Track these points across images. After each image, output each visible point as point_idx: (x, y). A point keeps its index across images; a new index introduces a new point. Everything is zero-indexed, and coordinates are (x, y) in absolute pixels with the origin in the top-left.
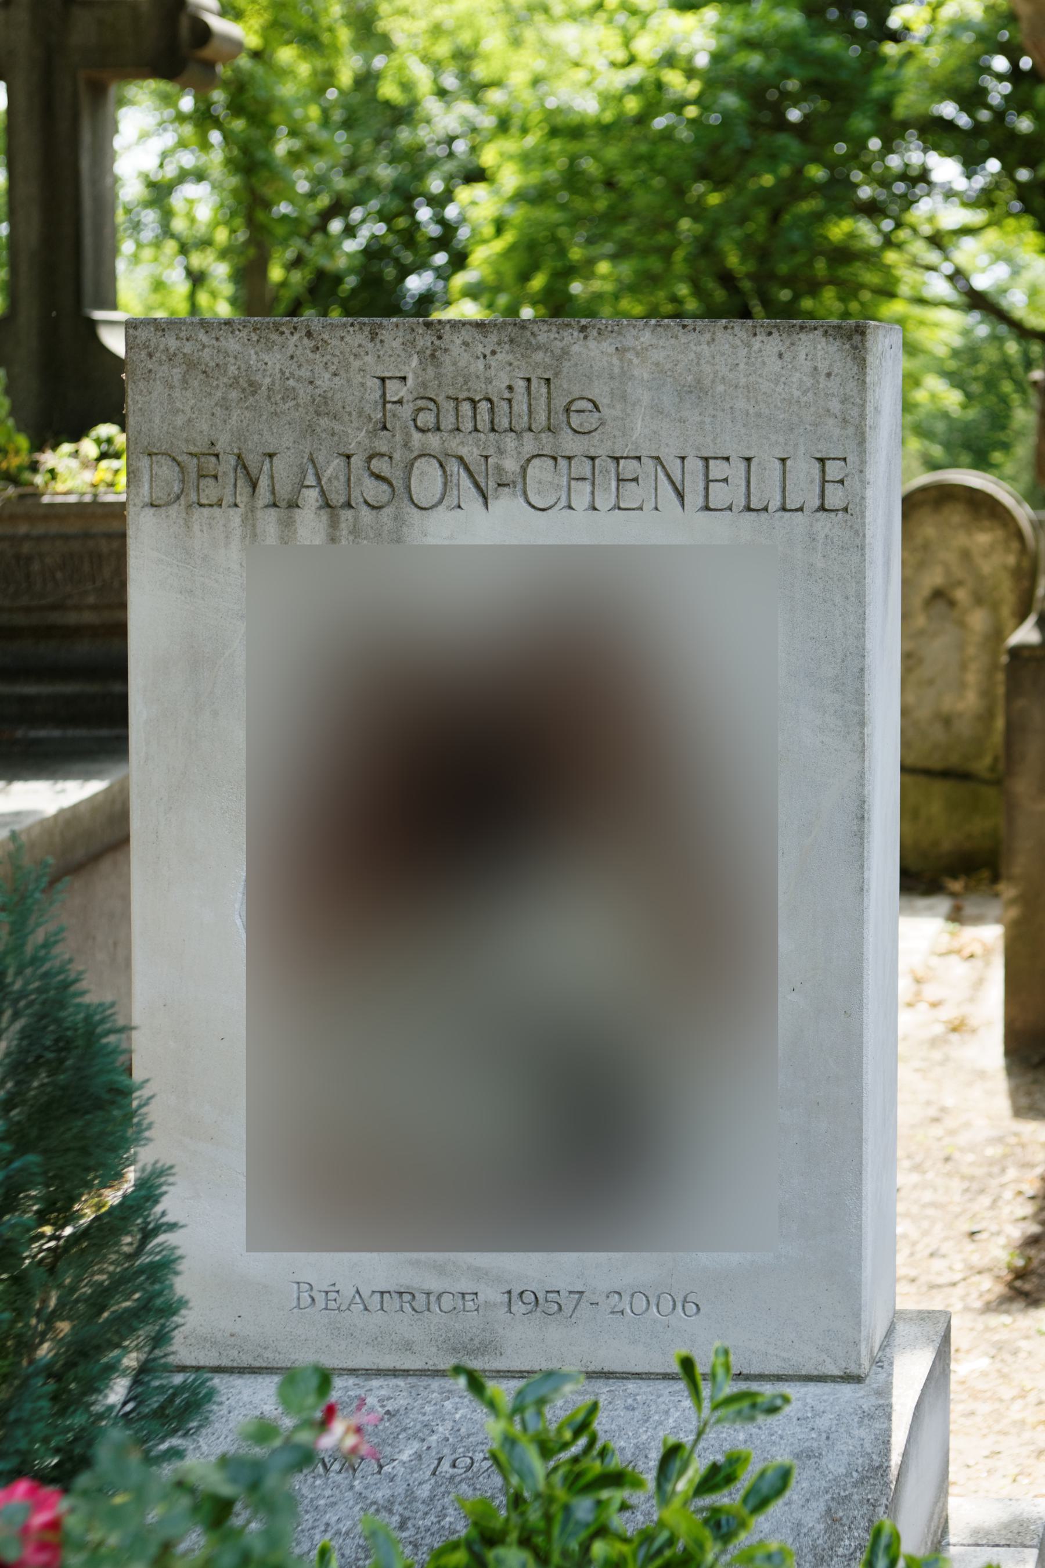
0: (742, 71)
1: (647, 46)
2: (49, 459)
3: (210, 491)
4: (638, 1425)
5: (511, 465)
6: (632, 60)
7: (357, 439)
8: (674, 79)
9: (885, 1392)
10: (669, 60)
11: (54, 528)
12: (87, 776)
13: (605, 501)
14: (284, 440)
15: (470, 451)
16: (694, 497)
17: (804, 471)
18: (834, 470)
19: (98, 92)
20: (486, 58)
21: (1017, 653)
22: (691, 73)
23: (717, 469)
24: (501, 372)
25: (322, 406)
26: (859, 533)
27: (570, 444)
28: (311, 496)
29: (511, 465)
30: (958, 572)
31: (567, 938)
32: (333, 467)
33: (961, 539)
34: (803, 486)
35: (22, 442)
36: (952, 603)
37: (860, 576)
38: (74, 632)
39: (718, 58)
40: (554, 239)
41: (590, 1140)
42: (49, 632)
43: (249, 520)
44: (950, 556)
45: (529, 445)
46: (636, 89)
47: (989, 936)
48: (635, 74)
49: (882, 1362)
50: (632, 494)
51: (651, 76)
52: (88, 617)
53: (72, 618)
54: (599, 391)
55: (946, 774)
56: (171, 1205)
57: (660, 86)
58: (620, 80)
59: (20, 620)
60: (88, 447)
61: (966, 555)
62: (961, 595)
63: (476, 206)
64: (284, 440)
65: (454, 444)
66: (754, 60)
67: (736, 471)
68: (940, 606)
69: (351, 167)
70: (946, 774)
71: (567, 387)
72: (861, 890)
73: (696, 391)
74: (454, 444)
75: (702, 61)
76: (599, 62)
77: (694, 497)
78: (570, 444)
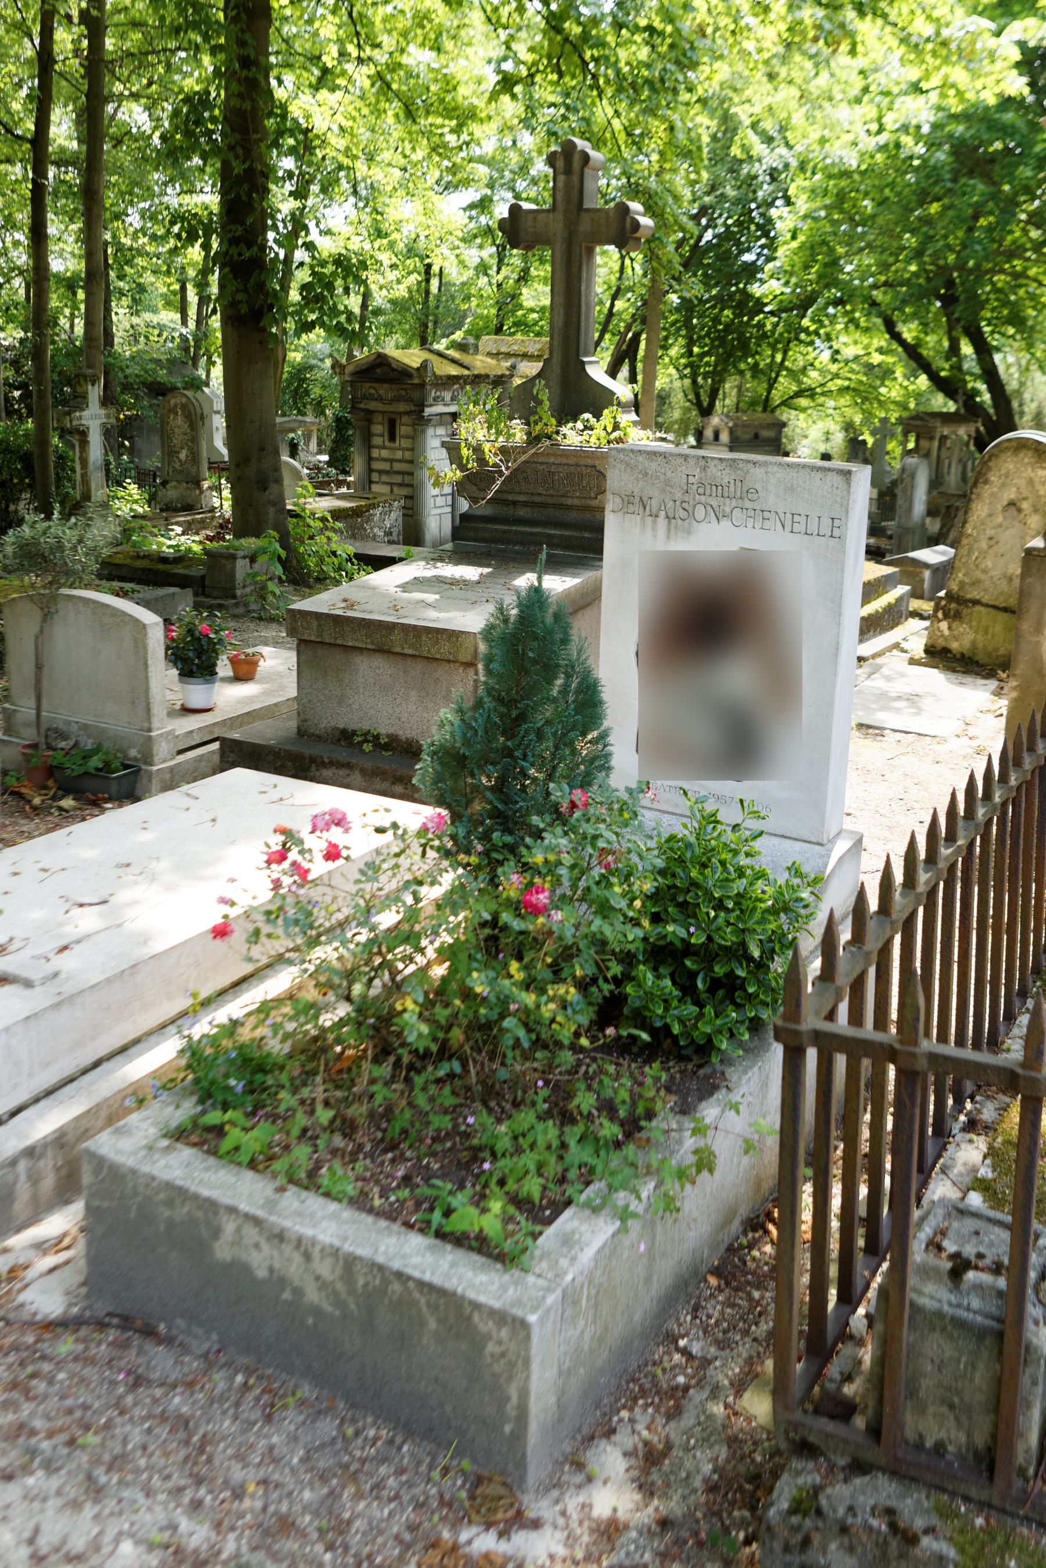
0: (951, 136)
1: (891, 121)
2: (564, 430)
3: (631, 508)
4: (729, 815)
5: (728, 510)
6: (880, 130)
7: (678, 495)
8: (907, 140)
9: (830, 850)
10: (905, 128)
11: (564, 461)
12: (574, 575)
13: (758, 525)
14: (655, 493)
15: (714, 503)
16: (788, 528)
17: (826, 522)
18: (837, 523)
19: (590, 252)
20: (793, 129)
21: (1029, 552)
22: (918, 138)
23: (797, 518)
24: (726, 476)
25: (668, 483)
26: (844, 546)
27: (748, 504)
28: (663, 514)
29: (728, 510)
30: (1025, 493)
31: (736, 677)
32: (670, 504)
33: (1029, 472)
34: (826, 530)
35: (554, 421)
36: (1020, 510)
37: (843, 563)
38: (570, 508)
39: (936, 127)
40: (824, 243)
41: (741, 745)
42: (560, 507)
43: (643, 520)
44: (1022, 483)
45: (734, 503)
46: (883, 148)
47: (1003, 704)
48: (883, 139)
49: (832, 841)
50: (767, 524)
51: (893, 137)
52: (576, 502)
53: (569, 502)
54: (758, 486)
55: (1005, 610)
56: (611, 739)
57: (898, 146)
58: (870, 143)
59: (549, 500)
60: (580, 425)
61: (1031, 482)
62: (1025, 505)
63: (783, 219)
64: (655, 493)
65: (710, 501)
66: (959, 129)
67: (803, 519)
68: (1012, 511)
69: (713, 188)
70: (1005, 610)
71: (748, 484)
72: (835, 674)
73: (791, 489)
74: (710, 501)
75: (926, 129)
76: (860, 130)
77: (788, 528)
78: (748, 504)
